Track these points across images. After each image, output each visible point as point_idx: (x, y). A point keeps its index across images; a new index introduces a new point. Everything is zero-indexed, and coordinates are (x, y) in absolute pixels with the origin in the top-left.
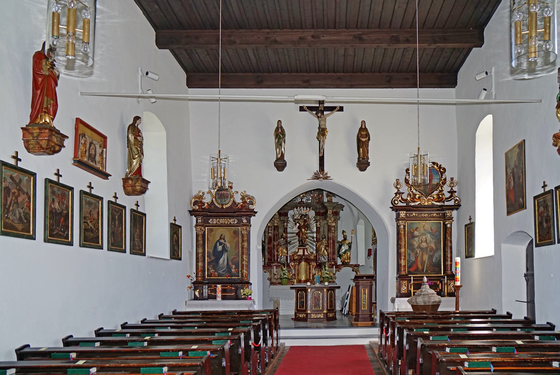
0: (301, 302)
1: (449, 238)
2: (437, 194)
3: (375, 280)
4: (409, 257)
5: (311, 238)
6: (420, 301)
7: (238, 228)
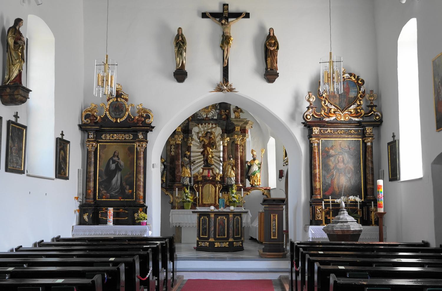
0: (204, 229)
1: (370, 165)
2: (355, 109)
3: (287, 205)
4: (324, 179)
5: (217, 158)
6: (338, 227)
7: (134, 144)
